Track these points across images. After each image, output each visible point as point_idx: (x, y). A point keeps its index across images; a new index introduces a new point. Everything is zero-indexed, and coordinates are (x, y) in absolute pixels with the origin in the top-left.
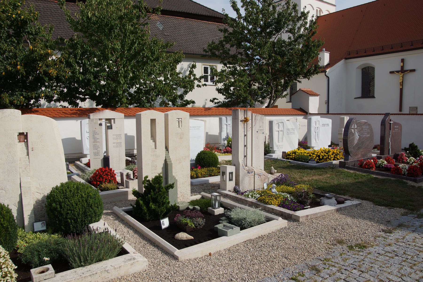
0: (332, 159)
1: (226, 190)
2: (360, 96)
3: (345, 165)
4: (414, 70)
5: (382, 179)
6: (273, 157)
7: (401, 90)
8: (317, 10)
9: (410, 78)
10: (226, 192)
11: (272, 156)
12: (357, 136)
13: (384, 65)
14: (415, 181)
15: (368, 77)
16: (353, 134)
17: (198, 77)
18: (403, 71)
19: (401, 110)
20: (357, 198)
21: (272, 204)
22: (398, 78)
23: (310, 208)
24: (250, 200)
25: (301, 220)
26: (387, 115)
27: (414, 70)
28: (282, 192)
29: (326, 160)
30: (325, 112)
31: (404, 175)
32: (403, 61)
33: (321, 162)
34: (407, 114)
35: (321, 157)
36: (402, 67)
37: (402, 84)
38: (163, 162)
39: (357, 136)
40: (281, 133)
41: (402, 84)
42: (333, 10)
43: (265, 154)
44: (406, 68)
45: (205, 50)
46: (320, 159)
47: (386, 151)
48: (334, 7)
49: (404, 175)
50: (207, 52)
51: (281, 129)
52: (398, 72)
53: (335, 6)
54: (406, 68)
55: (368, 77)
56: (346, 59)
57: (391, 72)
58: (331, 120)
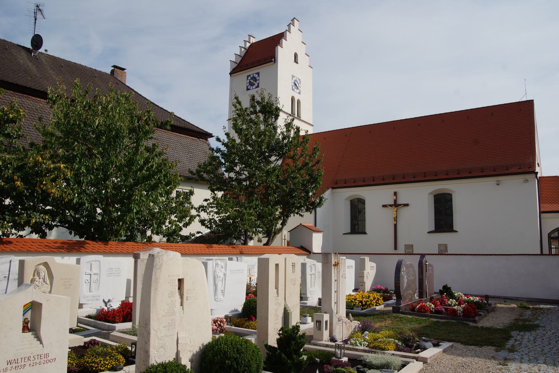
0: (375, 304)
1: (322, 340)
2: (349, 231)
3: (399, 310)
4: (407, 205)
5: (444, 322)
6: (308, 305)
7: (395, 226)
9: (403, 211)
10: (323, 342)
11: (306, 303)
12: (406, 281)
13: (375, 197)
14: (475, 322)
15: (357, 209)
16: (403, 277)
17: (196, 206)
18: (396, 205)
19: (396, 248)
20: (449, 341)
21: (389, 350)
22: (391, 212)
23: (421, 351)
24: (362, 348)
25: (429, 361)
26: (423, 256)
27: (407, 205)
28: (386, 337)
29: (369, 306)
30: (540, 253)
31: (460, 316)
32: (395, 194)
33: (365, 309)
34: (402, 254)
35: (364, 303)
36: (395, 201)
37: (396, 219)
38: (282, 311)
39: (406, 281)
40: (313, 276)
41: (396, 219)
43: (301, 300)
44: (399, 202)
45: (191, 172)
46: (363, 305)
47: (425, 296)
48: (312, 127)
49: (460, 316)
50: (194, 174)
51: (313, 272)
52: (391, 206)
53: (312, 125)
54: (399, 202)
55: (357, 209)
56: (333, 188)
57: (384, 206)
58: (354, 261)
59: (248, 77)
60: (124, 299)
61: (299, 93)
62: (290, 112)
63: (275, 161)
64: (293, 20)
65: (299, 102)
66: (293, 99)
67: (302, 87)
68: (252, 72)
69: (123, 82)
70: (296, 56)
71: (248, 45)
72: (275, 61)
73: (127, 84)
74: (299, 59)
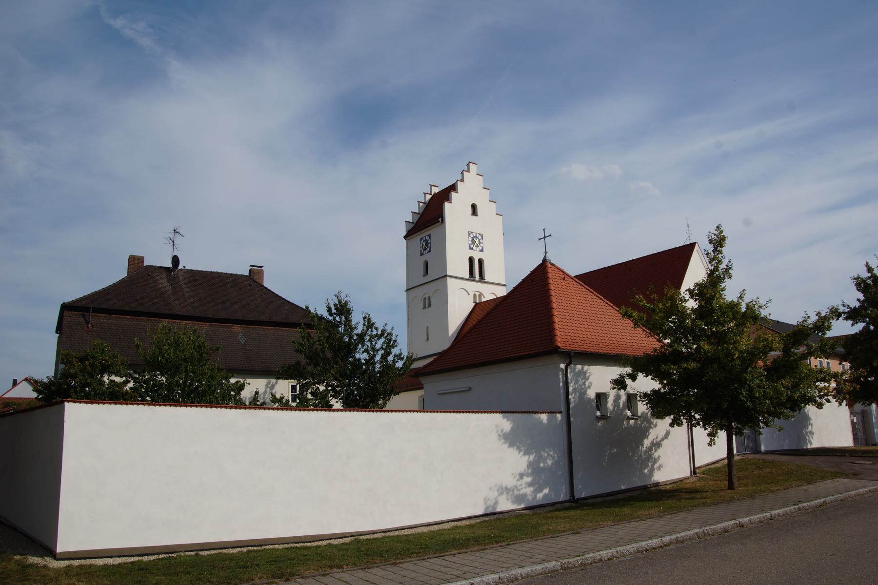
8: (475, 295)
42: (502, 292)
53: (505, 285)
59: (421, 239)
60: (716, 439)
61: (482, 250)
62: (467, 276)
63: (231, 405)
64: (468, 165)
65: (481, 262)
66: (471, 260)
67: (486, 243)
68: (424, 234)
69: (260, 282)
70: (474, 207)
71: (429, 197)
72: (443, 221)
73: (265, 284)
74: (479, 210)
